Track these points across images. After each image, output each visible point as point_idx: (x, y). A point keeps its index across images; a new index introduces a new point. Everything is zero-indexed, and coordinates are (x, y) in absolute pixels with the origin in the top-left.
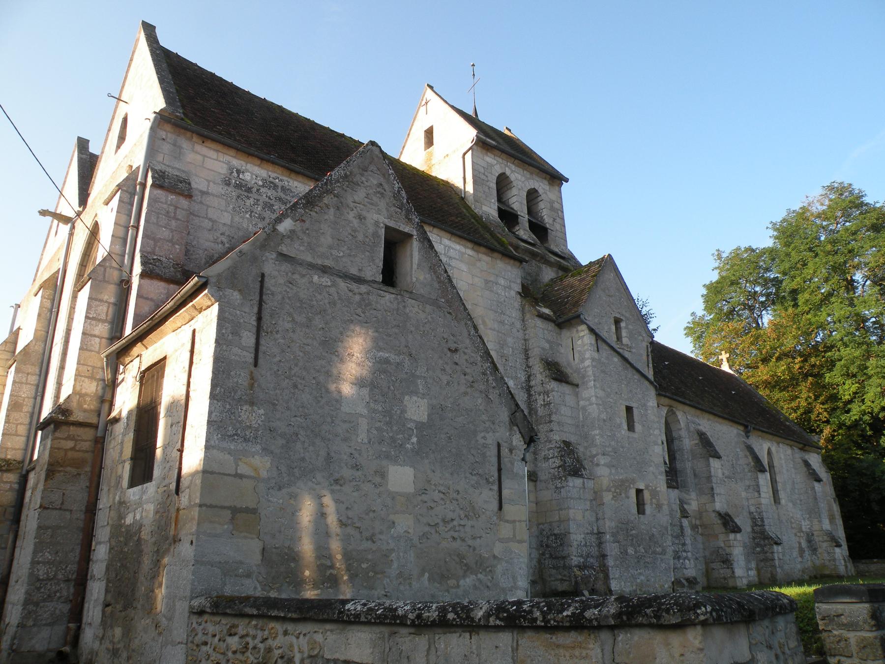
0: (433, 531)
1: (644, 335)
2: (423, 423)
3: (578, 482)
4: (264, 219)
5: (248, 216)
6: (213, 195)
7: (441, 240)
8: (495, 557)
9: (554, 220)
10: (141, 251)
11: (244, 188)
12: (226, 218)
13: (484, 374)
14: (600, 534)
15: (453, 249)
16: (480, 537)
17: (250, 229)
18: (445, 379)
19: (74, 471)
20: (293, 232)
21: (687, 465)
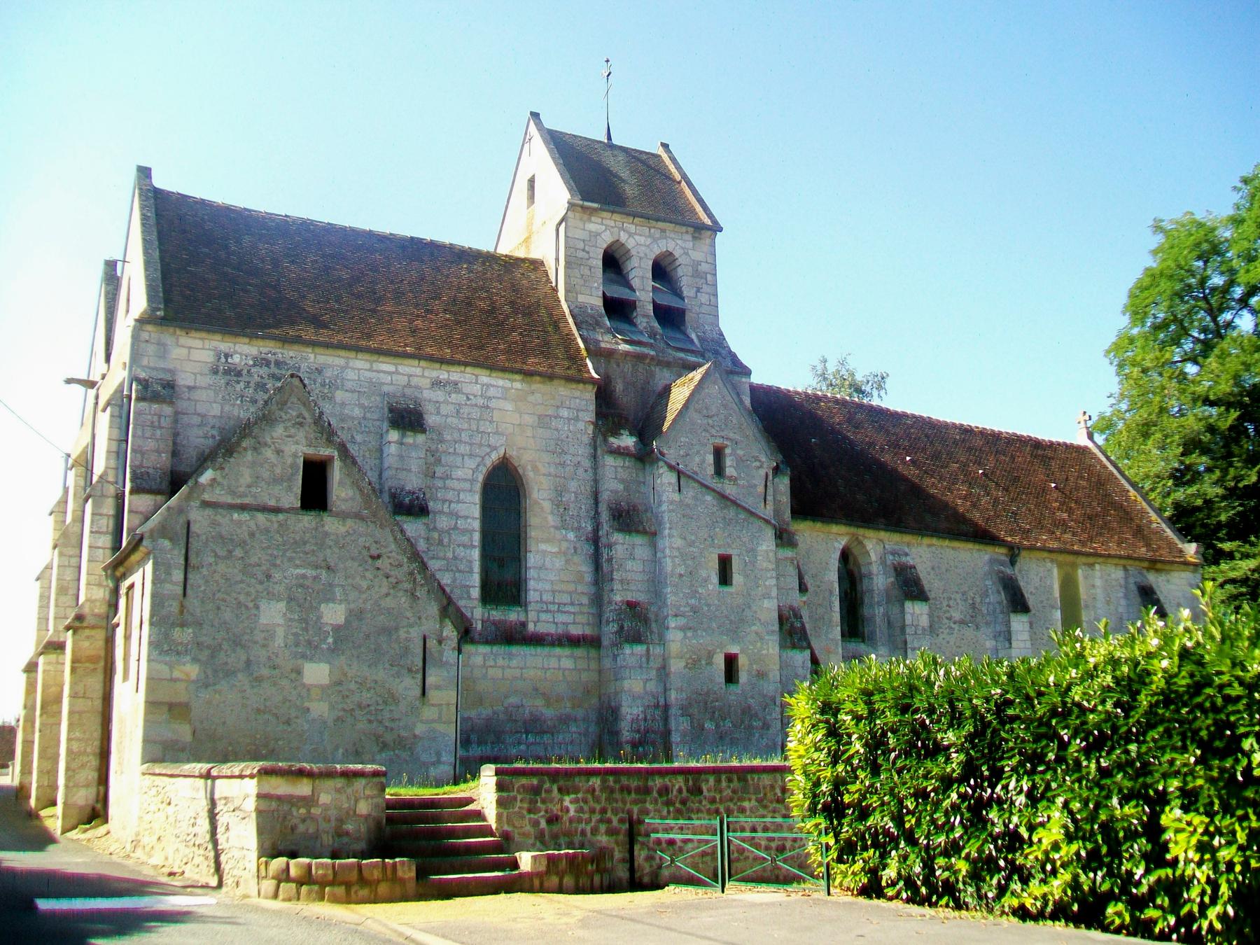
0: (349, 715)
1: (764, 460)
2: (340, 626)
3: (640, 649)
4: (256, 402)
5: (238, 402)
6: (201, 388)
7: (477, 380)
8: (415, 736)
9: (698, 290)
10: (131, 466)
11: (234, 373)
12: (216, 410)
13: (411, 574)
14: (666, 707)
15: (493, 386)
16: (399, 720)
17: (241, 416)
18: (364, 584)
19: (92, 666)
20: (214, 480)
21: (876, 612)
